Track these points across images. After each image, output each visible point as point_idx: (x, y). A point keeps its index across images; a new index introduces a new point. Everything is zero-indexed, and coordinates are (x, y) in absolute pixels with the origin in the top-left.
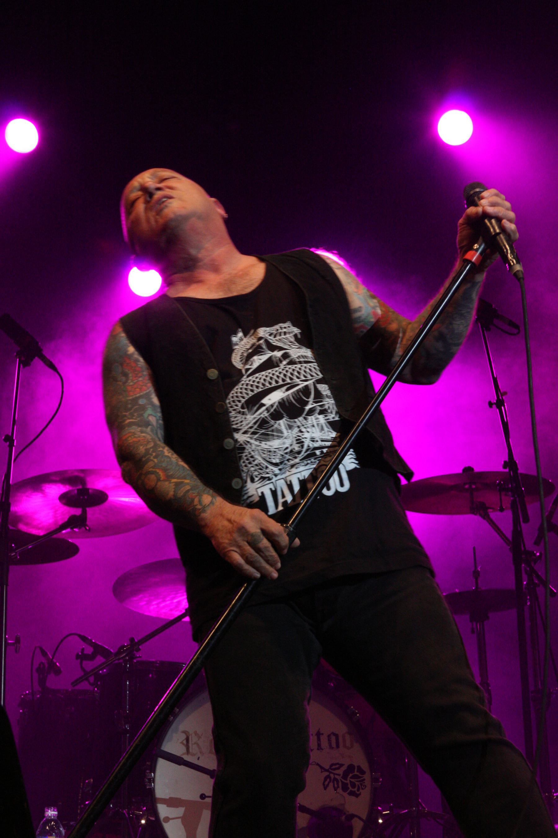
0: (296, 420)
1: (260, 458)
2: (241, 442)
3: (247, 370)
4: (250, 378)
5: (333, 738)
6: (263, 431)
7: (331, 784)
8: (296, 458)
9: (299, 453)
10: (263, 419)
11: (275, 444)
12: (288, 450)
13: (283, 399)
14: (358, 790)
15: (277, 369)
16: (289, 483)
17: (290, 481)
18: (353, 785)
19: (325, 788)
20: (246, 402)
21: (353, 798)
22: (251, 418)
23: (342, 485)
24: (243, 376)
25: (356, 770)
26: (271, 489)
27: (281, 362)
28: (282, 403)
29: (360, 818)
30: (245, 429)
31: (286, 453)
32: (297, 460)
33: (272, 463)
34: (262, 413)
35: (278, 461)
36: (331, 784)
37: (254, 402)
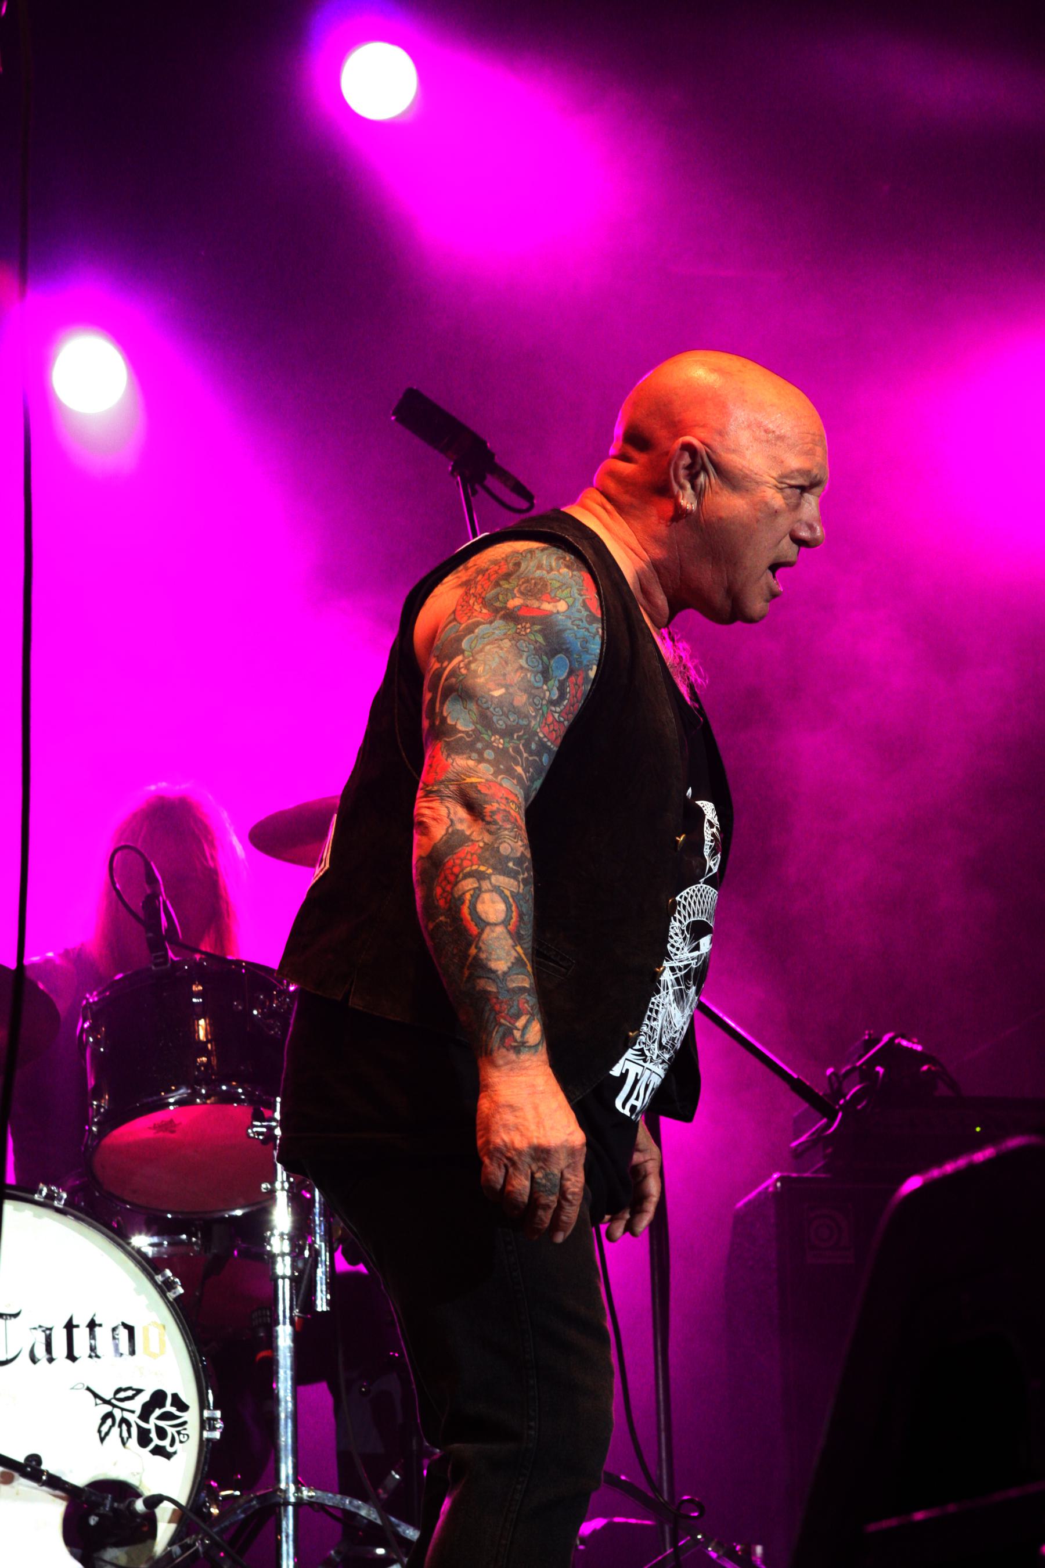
5: (123, 1333)
14: (172, 1444)
36: (116, 1430)
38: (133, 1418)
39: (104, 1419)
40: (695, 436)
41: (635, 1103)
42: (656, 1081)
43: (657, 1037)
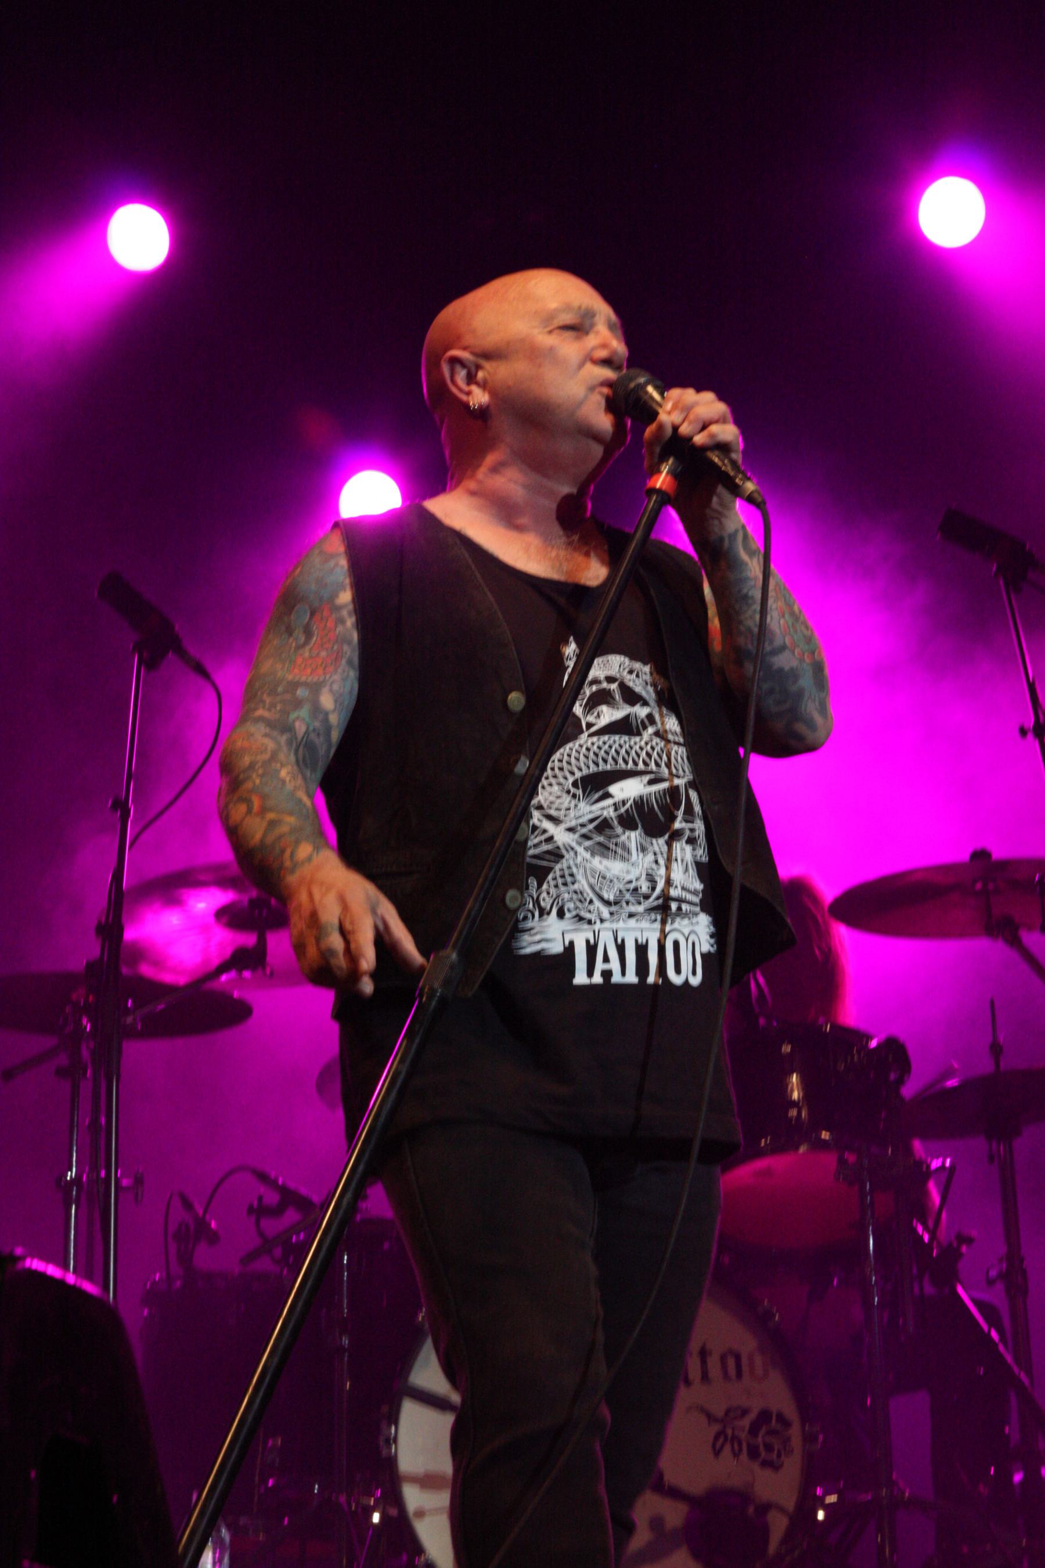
0: (654, 841)
1: (584, 882)
2: (560, 844)
3: (589, 725)
4: (595, 739)
5: (731, 1362)
6: (601, 839)
7: (727, 1449)
8: (640, 903)
9: (647, 897)
10: (605, 819)
11: (614, 867)
12: (632, 886)
13: (641, 797)
14: (779, 1456)
15: (637, 739)
16: (619, 941)
17: (623, 941)
18: (769, 1448)
19: (717, 1453)
20: (583, 779)
21: (768, 1473)
22: (587, 810)
23: (694, 973)
24: (582, 732)
25: (774, 1421)
26: (588, 942)
27: (645, 728)
28: (640, 803)
29: (781, 1509)
30: (573, 823)
31: (628, 890)
32: (640, 909)
33: (601, 898)
34: (605, 809)
35: (612, 898)
36: (727, 1449)
37: (595, 784)
38: (743, 1435)
39: (717, 1438)
40: (465, 348)
41: (606, 967)
42: (706, 945)
43: (591, 895)
